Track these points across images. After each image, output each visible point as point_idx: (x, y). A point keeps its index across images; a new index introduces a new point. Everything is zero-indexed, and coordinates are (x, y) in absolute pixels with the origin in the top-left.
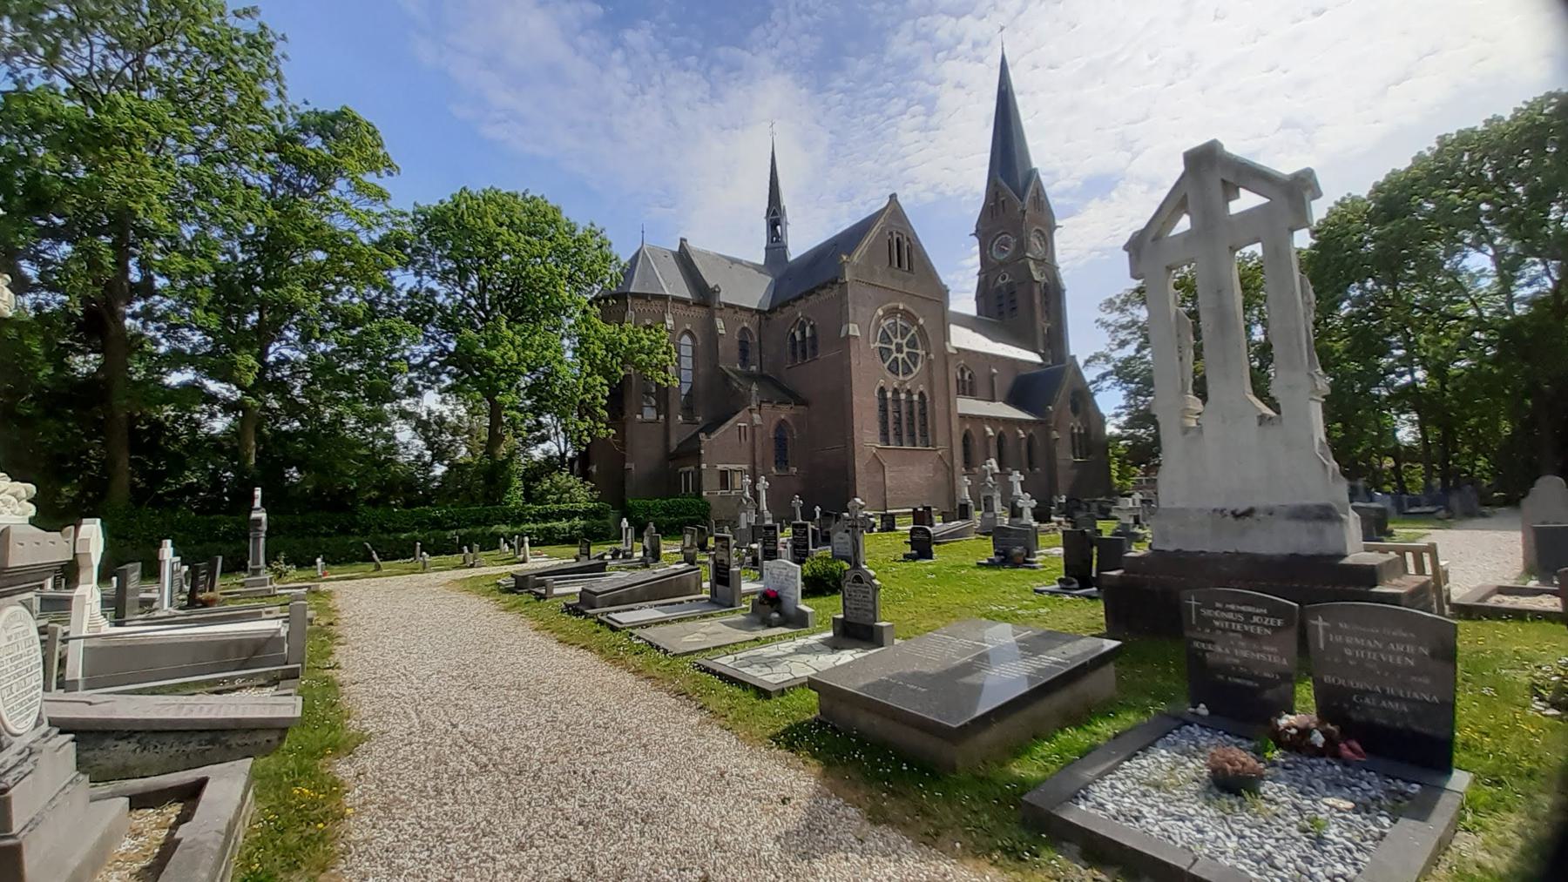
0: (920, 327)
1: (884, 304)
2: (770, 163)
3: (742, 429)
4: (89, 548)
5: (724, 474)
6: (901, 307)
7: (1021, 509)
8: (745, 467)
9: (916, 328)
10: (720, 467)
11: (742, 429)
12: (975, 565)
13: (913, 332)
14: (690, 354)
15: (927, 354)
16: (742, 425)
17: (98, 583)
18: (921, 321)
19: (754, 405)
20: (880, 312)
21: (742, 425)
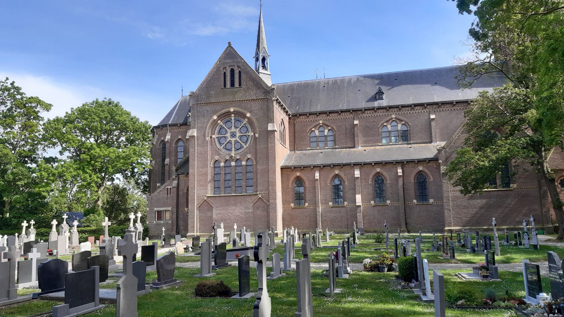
0: (248, 118)
1: (218, 111)
2: (258, 28)
3: (169, 190)
4: (306, 252)
5: (159, 213)
6: (232, 110)
7: (23, 226)
8: (170, 209)
9: (246, 120)
10: (156, 209)
11: (169, 190)
12: (50, 249)
13: (221, 124)
14: (178, 153)
15: (254, 134)
16: (169, 187)
17: (524, 280)
18: (248, 115)
19: (174, 177)
20: (215, 117)
21: (169, 187)
